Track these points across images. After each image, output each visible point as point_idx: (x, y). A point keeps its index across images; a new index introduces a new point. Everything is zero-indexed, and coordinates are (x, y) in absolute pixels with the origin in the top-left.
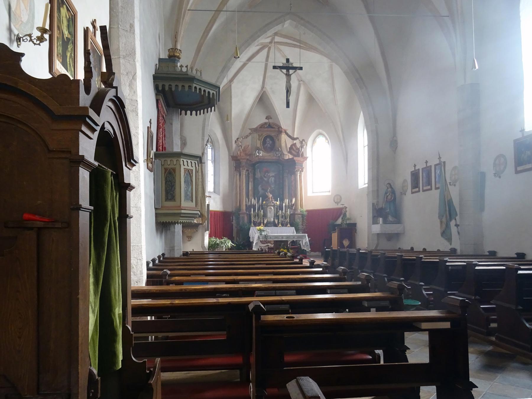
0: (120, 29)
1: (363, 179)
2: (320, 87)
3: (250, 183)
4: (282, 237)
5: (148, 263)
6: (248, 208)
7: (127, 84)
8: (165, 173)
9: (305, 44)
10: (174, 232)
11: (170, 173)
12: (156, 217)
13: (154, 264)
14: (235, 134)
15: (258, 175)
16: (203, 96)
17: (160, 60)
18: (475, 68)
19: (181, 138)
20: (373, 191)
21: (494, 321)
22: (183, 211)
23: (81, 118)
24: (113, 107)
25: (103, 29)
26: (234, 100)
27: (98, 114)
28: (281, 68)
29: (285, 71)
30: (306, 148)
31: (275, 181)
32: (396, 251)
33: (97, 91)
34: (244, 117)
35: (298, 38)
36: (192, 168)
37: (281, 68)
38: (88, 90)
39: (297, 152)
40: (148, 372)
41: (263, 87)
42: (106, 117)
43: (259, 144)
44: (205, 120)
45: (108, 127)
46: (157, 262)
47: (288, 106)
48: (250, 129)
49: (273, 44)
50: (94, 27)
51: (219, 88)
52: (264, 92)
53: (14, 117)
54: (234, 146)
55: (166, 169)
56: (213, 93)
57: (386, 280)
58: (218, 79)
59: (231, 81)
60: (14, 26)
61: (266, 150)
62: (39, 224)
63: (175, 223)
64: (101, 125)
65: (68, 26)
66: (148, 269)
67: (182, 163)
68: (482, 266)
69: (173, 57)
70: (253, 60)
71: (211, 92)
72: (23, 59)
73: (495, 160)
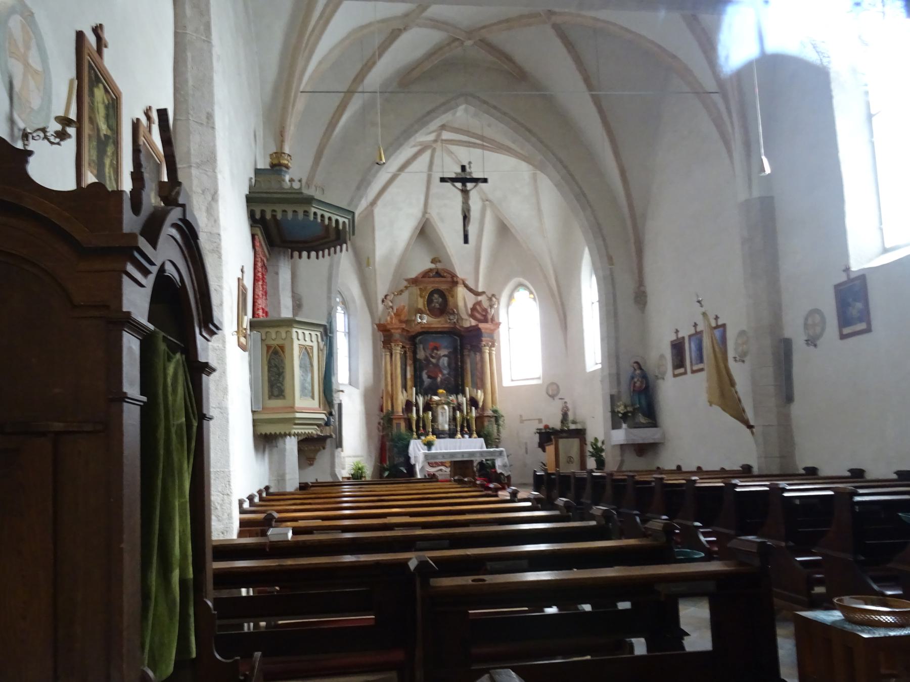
0: (191, 122)
1: (593, 355)
2: (519, 211)
3: (408, 368)
4: (463, 454)
5: (241, 502)
6: (409, 405)
7: (204, 208)
8: (268, 352)
9: (491, 141)
10: (284, 450)
11: (276, 353)
12: (254, 426)
13: (252, 503)
14: (382, 288)
15: (421, 355)
16: (327, 228)
17: (257, 172)
18: (764, 171)
19: (293, 297)
20: (610, 375)
21: (820, 582)
22: (298, 415)
23: (126, 252)
24: (178, 237)
25: (162, 113)
26: (379, 234)
27: (154, 244)
28: (453, 180)
29: (459, 185)
30: (498, 308)
31: (449, 364)
32: (650, 472)
33: (152, 210)
34: (395, 260)
35: (480, 133)
36: (311, 344)
37: (453, 180)
38: (136, 205)
39: (484, 314)
40: (242, 678)
41: (425, 212)
42: (166, 253)
43: (421, 303)
44: (331, 267)
45: (170, 270)
46: (256, 500)
47: (466, 241)
48: (406, 280)
49: (439, 143)
50: (149, 118)
51: (353, 213)
52: (427, 219)
53: (14, 252)
54: (381, 307)
55: (269, 347)
56: (344, 222)
57: (638, 519)
58: (352, 200)
59: (373, 203)
60: (20, 117)
61: (433, 312)
62: (58, 426)
63: (285, 435)
64: (159, 264)
65: (107, 117)
66: (242, 511)
67: (294, 336)
68: (794, 491)
69: (277, 167)
70: (406, 170)
71: (341, 220)
72: (31, 159)
73: (806, 319)
